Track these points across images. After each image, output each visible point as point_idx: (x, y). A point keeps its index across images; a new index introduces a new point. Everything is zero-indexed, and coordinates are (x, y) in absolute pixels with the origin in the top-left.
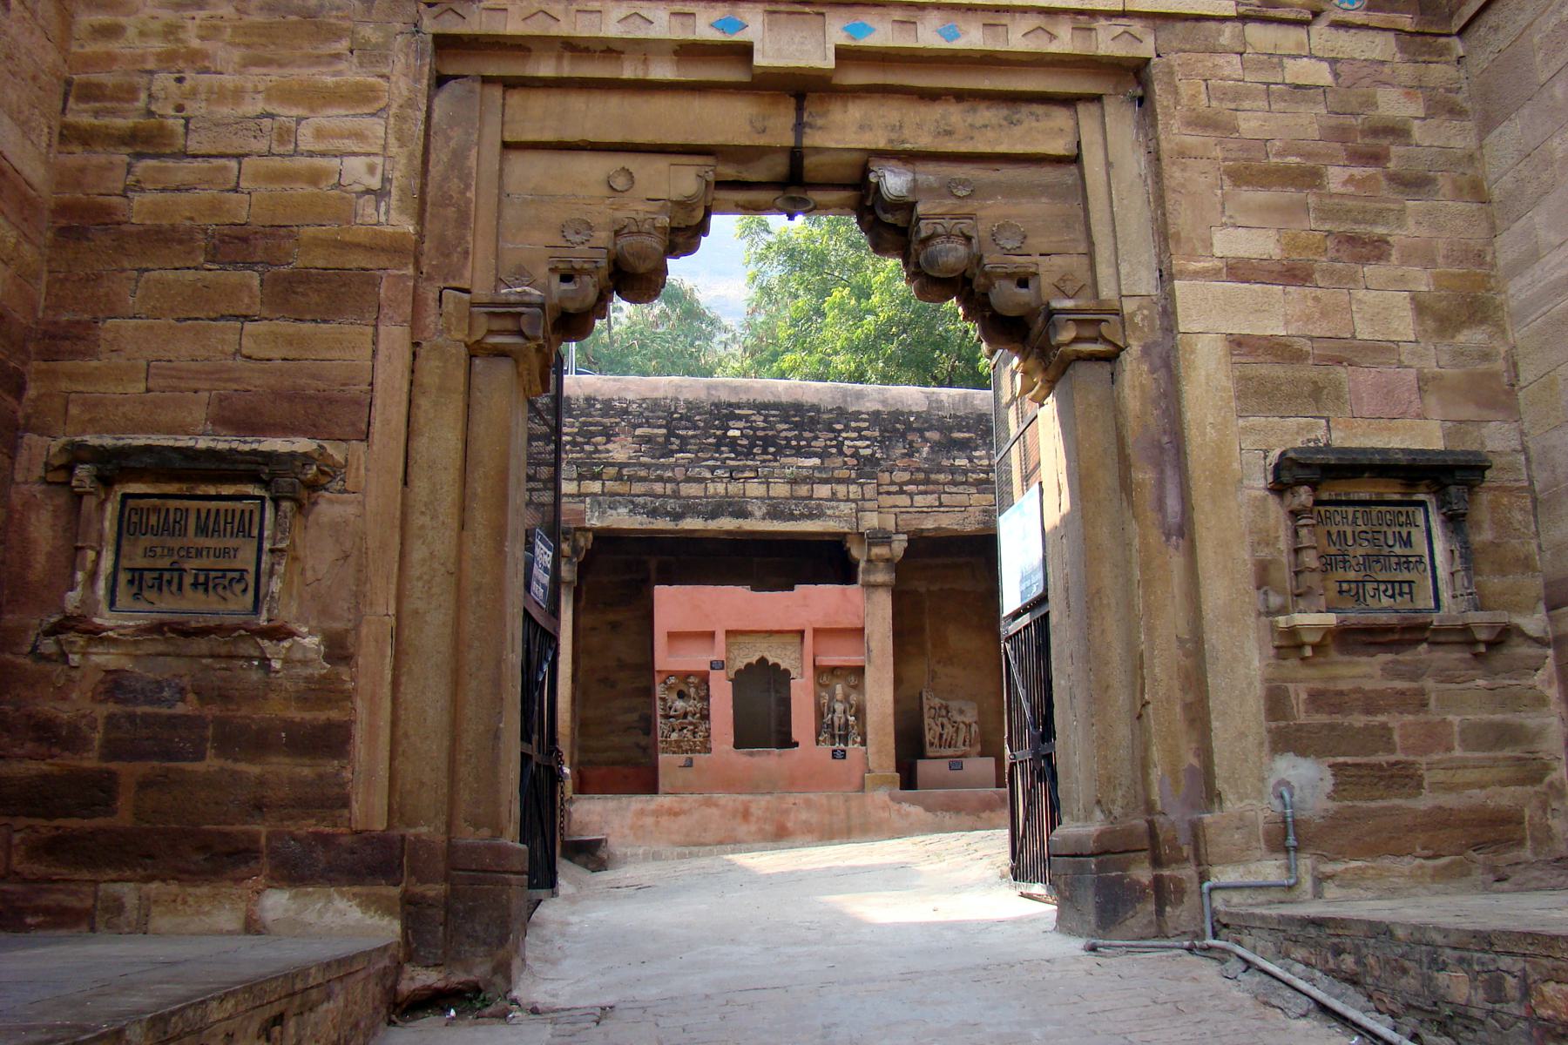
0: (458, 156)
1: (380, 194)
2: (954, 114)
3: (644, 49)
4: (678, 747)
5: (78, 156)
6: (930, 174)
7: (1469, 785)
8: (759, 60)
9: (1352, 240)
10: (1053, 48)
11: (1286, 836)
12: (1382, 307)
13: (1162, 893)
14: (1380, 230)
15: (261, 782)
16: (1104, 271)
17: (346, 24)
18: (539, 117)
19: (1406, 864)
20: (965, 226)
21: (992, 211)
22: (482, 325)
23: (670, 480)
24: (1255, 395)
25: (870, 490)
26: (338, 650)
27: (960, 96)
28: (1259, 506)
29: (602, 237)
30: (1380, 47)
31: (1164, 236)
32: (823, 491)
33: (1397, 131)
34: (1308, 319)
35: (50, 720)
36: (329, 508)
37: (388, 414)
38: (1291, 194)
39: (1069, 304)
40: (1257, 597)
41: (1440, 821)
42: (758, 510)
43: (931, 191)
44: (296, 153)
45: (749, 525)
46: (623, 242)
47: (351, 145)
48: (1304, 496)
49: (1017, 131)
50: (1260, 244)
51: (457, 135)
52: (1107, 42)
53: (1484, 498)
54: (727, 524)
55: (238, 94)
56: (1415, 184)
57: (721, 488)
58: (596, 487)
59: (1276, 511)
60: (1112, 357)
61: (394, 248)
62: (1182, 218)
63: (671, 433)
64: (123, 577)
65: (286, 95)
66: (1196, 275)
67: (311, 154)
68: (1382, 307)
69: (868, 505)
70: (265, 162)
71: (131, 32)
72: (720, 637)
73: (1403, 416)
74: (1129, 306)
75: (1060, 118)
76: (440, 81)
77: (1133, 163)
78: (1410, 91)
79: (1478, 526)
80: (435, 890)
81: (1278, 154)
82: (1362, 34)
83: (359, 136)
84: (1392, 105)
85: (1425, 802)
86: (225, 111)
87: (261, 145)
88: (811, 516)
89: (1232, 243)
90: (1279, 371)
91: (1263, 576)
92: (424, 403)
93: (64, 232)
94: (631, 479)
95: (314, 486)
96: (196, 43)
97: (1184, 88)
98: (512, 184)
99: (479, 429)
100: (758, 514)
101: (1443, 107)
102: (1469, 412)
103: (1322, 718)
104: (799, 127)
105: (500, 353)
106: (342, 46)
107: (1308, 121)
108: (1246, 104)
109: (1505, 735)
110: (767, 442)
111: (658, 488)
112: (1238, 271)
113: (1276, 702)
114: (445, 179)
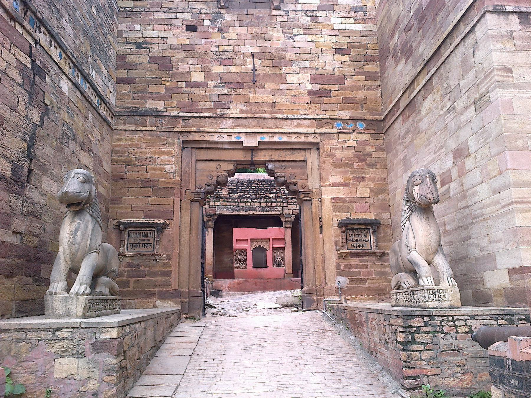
0: (188, 164)
1: (173, 173)
2: (282, 153)
3: (222, 143)
4: (239, 268)
5: (115, 166)
6: (278, 164)
7: (376, 283)
8: (244, 145)
9: (358, 177)
10: (300, 141)
11: (340, 291)
12: (363, 191)
13: (318, 301)
14: (364, 175)
15: (155, 281)
16: (310, 183)
17: (165, 138)
18: (203, 155)
19: (362, 297)
20: (284, 175)
21: (289, 171)
22: (193, 196)
23: (236, 202)
24: (336, 209)
25: (286, 204)
26: (169, 258)
27: (283, 149)
28: (336, 229)
29: (215, 178)
30: (367, 137)
31: (321, 178)
32: (274, 204)
33: (370, 155)
34: (348, 194)
35: (97, 265)
36: (166, 232)
37: (176, 215)
38: (346, 169)
39: (303, 190)
40: (335, 247)
41: (370, 289)
42: (257, 208)
43: (277, 168)
44: (157, 164)
45: (256, 213)
46: (219, 178)
47: (167, 163)
48: (344, 229)
49: (294, 156)
50: (338, 179)
51: (187, 159)
52: (311, 139)
53: (382, 228)
54: (251, 212)
55: (146, 153)
56: (372, 165)
57: (249, 204)
58: (218, 204)
59: (339, 231)
60: (311, 200)
61: (176, 183)
62: (324, 175)
63: (238, 188)
64: (129, 245)
65: (155, 153)
66: (326, 186)
67: (160, 165)
68: (363, 191)
69: (285, 208)
70: (152, 166)
71: (124, 140)
72: (249, 240)
73: (366, 212)
74: (314, 191)
75: (303, 153)
76: (184, 148)
77: (316, 163)
78: (372, 146)
79: (380, 233)
80: (187, 300)
81: (345, 161)
82: (363, 135)
83: (169, 161)
84: (369, 149)
85: (367, 286)
86: (143, 156)
87: (151, 163)
88: (271, 211)
89: (333, 179)
90: (341, 204)
91: (336, 244)
92: (183, 211)
93: (114, 180)
94: (226, 201)
95: (164, 228)
96: (136, 142)
97: (326, 148)
98: (198, 168)
99: (193, 216)
100: (258, 210)
101: (380, 149)
102: (380, 211)
103: (347, 270)
104: (252, 156)
105: (197, 201)
106: (165, 143)
107: (350, 153)
108: (338, 151)
109: (383, 273)
110: (262, 190)
111: (234, 204)
112: (334, 185)
113: (338, 266)
114: (185, 168)
